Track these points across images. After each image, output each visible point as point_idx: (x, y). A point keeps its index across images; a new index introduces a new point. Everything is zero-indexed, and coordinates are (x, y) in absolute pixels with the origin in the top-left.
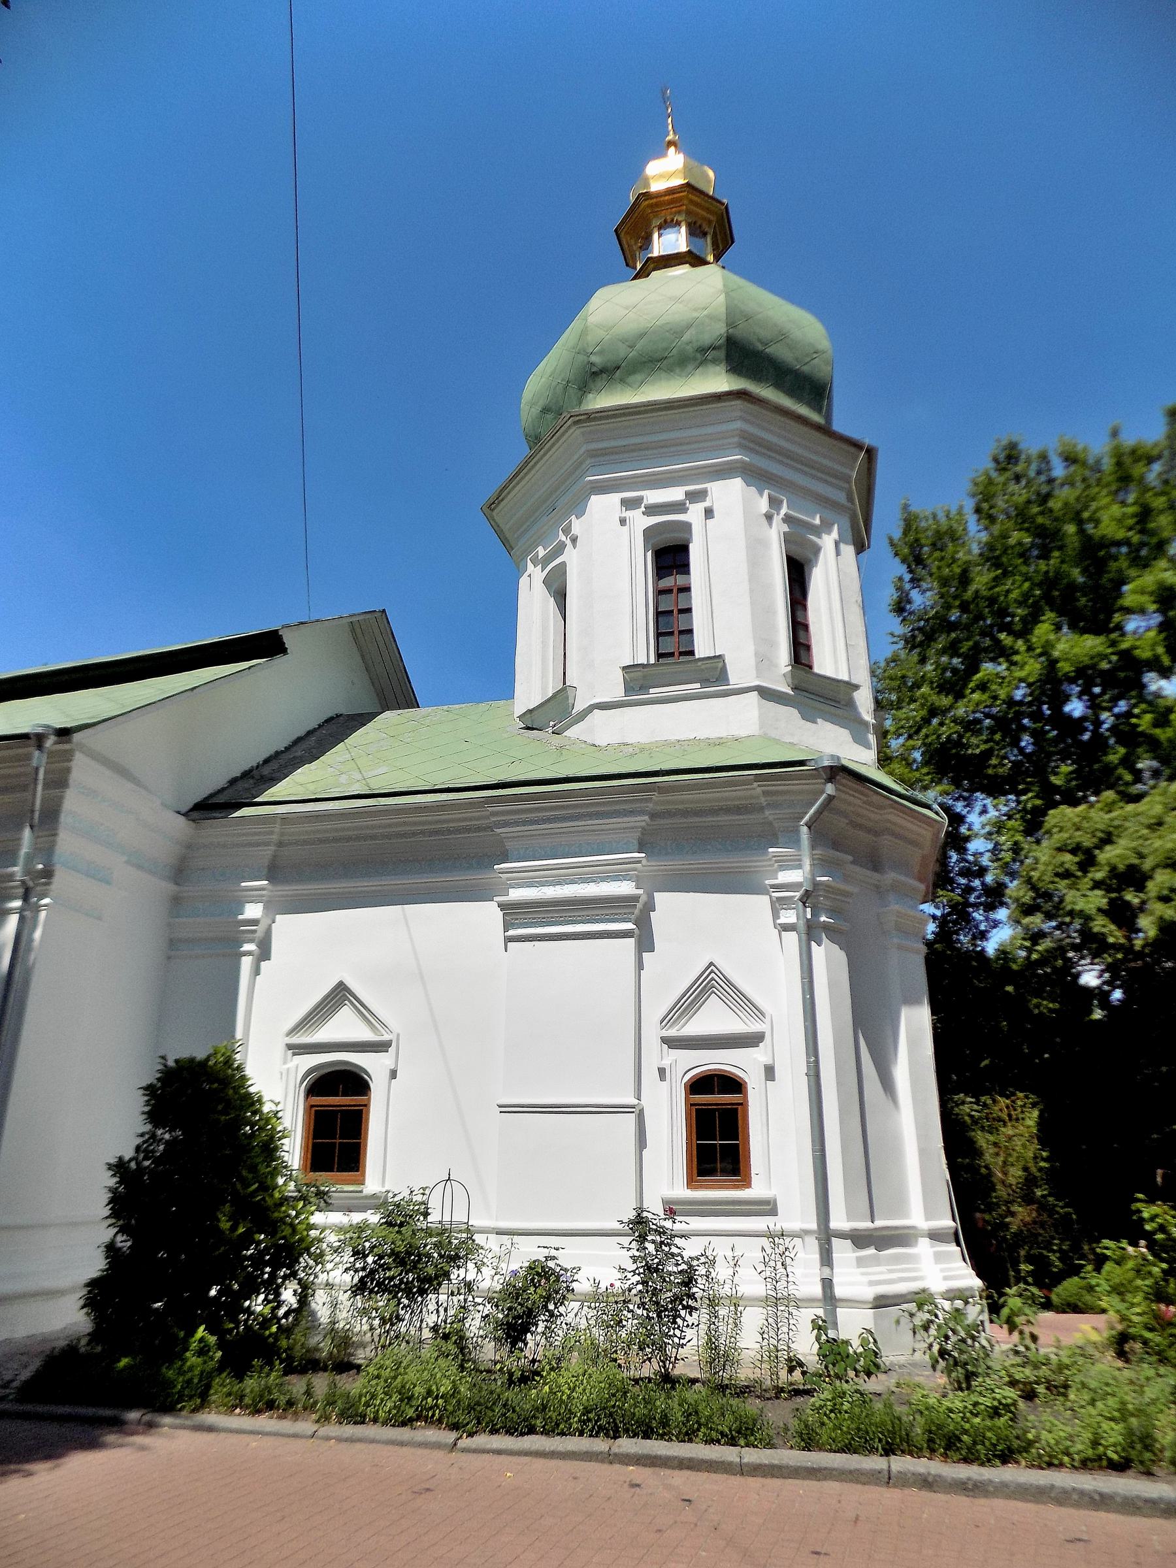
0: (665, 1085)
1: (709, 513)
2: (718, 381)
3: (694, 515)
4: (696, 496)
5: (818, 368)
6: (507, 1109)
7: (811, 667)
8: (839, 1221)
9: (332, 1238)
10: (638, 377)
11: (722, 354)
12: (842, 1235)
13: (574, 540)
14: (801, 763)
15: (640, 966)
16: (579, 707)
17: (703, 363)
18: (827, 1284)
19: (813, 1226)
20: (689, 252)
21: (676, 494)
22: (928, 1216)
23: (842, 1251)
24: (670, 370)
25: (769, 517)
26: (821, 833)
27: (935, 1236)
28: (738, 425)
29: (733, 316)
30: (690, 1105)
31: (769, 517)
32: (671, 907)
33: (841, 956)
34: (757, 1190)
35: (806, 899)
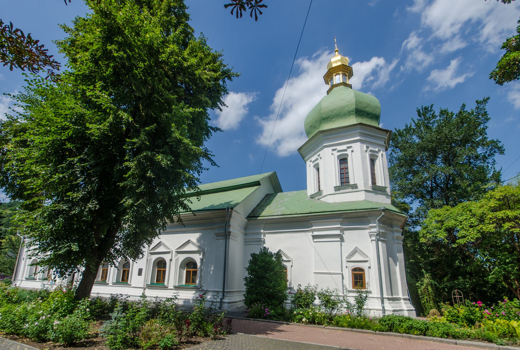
0: (347, 269)
1: (352, 151)
2: (353, 120)
3: (349, 152)
4: (350, 147)
5: (377, 112)
7: (376, 184)
8: (385, 296)
10: (334, 119)
11: (354, 112)
12: (386, 298)
13: (321, 158)
14: (377, 208)
15: (341, 245)
17: (349, 115)
18: (383, 307)
19: (380, 296)
20: (343, 83)
21: (344, 147)
22: (403, 295)
23: (386, 301)
24: (342, 117)
25: (366, 151)
26: (381, 221)
27: (405, 299)
28: (359, 131)
29: (357, 102)
30: (353, 273)
31: (366, 151)
32: (347, 235)
33: (385, 245)
35: (377, 235)
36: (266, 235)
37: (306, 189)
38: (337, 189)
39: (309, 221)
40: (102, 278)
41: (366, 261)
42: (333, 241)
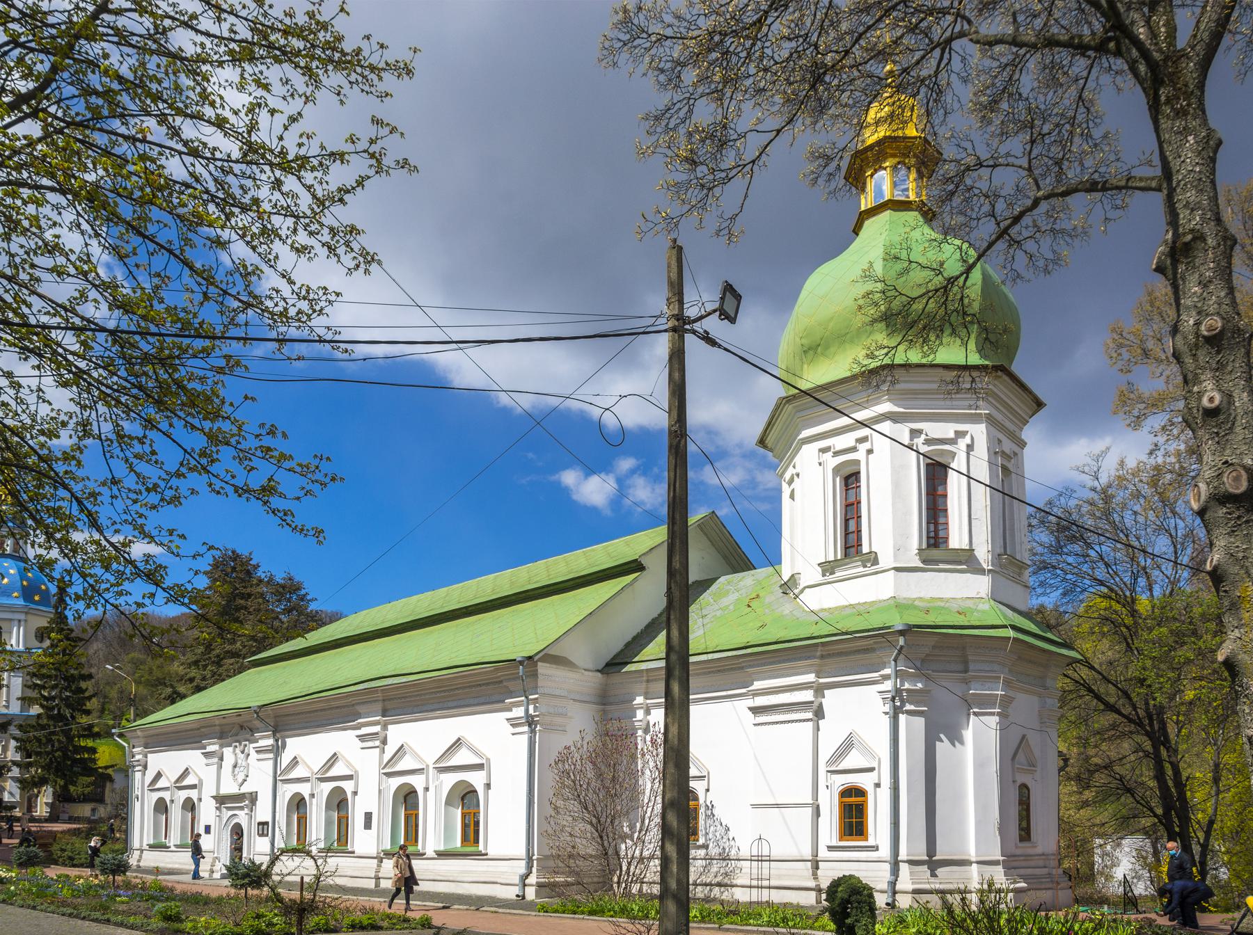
6: (754, 806)
8: (903, 855)
9: (15, 594)
14: (889, 628)
16: (803, 584)
30: (841, 803)
34: (871, 842)
36: (826, 692)
37: (779, 561)
38: (828, 568)
39: (742, 668)
40: (298, 839)
41: (871, 770)
42: (782, 722)
